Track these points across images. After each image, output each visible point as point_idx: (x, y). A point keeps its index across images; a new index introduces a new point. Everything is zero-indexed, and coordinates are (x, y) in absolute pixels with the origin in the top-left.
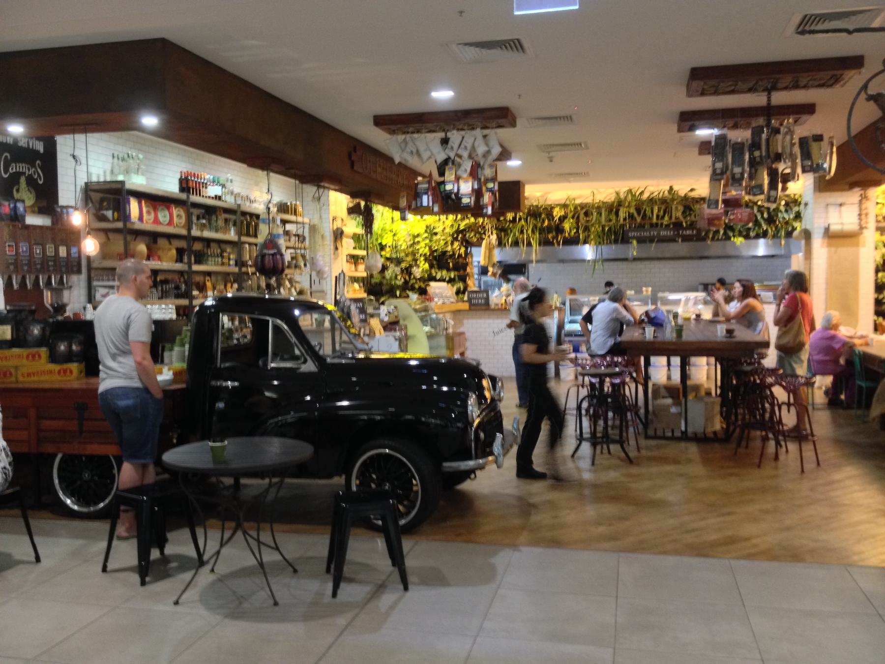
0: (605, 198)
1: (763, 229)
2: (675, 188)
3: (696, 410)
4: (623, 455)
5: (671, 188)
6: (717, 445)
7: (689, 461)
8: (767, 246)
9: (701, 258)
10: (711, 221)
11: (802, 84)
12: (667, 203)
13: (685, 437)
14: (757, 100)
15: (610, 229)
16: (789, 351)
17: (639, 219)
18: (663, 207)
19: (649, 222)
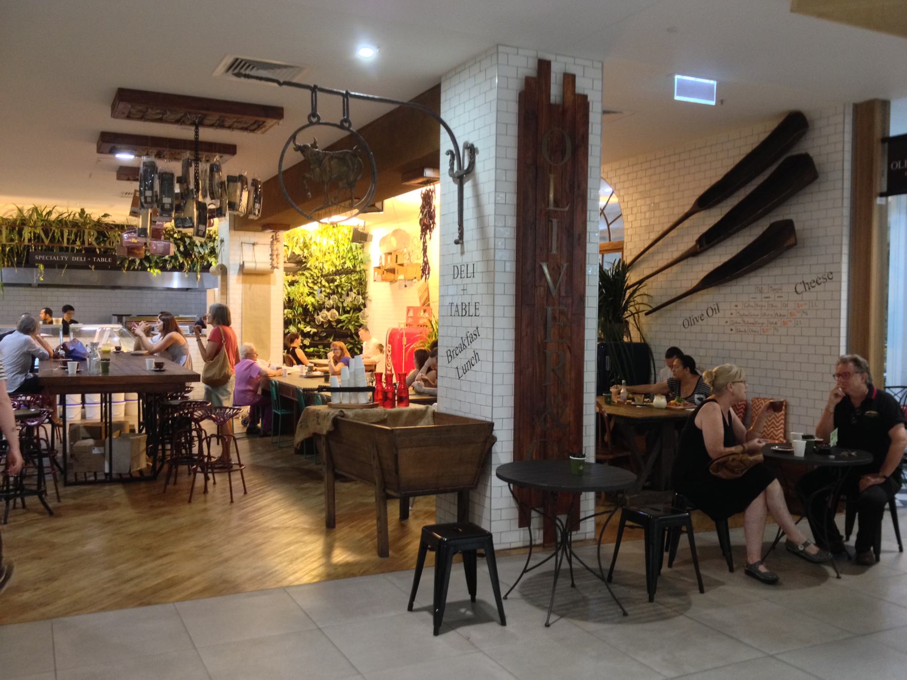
0: (6, 213)
1: (179, 262)
2: (87, 211)
3: (120, 448)
4: (42, 507)
5: (83, 211)
6: (143, 485)
7: (118, 505)
8: (182, 278)
9: (115, 288)
10: (132, 249)
11: (227, 124)
12: (79, 227)
13: (110, 479)
14: (186, 133)
15: (11, 250)
16: (216, 383)
17: (47, 242)
18: (74, 230)
19: (58, 245)
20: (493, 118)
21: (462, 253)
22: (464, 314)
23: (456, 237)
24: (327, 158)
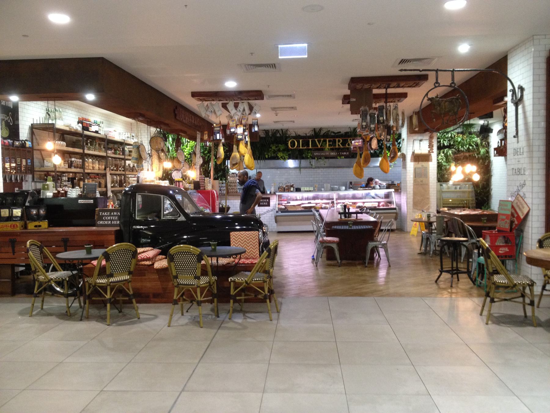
20: (531, 73)
21: (518, 142)
22: (519, 174)
23: (515, 134)
24: (443, 102)
